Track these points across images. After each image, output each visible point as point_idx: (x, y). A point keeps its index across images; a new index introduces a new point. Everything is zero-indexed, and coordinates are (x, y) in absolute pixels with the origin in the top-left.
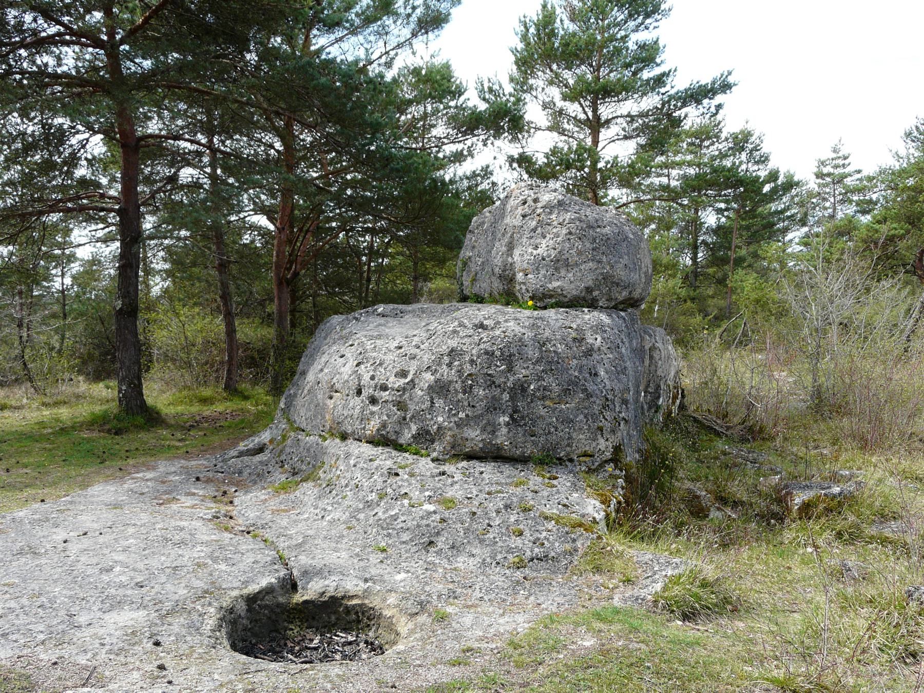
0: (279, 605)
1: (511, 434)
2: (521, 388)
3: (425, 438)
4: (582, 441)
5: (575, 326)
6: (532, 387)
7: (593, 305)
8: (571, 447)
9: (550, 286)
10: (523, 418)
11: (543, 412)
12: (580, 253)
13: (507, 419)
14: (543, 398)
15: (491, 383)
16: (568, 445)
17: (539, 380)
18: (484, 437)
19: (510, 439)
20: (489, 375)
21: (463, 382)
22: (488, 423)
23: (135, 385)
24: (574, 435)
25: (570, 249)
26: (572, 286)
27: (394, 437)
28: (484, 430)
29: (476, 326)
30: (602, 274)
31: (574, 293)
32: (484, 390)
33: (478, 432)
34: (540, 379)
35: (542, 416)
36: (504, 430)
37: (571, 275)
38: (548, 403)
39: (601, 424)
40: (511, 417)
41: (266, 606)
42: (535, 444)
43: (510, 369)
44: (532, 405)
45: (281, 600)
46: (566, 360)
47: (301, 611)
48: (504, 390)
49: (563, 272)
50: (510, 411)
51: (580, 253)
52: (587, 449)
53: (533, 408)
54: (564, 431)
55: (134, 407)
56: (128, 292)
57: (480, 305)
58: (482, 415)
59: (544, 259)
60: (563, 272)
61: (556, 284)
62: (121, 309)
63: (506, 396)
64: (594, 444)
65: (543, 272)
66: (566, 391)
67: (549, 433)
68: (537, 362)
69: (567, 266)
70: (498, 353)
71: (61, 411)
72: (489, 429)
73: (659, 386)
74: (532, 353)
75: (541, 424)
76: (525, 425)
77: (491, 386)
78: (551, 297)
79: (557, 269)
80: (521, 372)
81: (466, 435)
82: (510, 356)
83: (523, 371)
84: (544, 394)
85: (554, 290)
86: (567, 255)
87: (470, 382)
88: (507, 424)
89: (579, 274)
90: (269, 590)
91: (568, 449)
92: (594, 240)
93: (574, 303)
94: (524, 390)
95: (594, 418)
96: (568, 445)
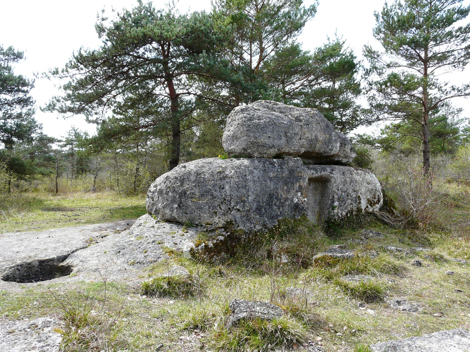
0: (54, 265)
2: (184, 193)
3: (157, 212)
4: (205, 218)
5: (223, 166)
9: (230, 148)
10: (183, 206)
11: (190, 203)
13: (177, 206)
14: (192, 198)
15: (174, 191)
16: (199, 219)
22: (171, 207)
24: (202, 215)
31: (239, 151)
34: (192, 189)
36: (175, 211)
37: (238, 143)
38: (194, 200)
39: (216, 211)
40: (179, 205)
41: (48, 265)
42: (186, 217)
45: (55, 264)
46: (208, 181)
47: (60, 269)
49: (235, 141)
51: (241, 133)
52: (208, 221)
54: (197, 213)
58: (170, 204)
61: (232, 147)
64: (212, 219)
65: (228, 142)
66: (202, 195)
67: (192, 213)
69: (237, 139)
71: (137, 202)
72: (172, 210)
73: (334, 196)
74: (193, 178)
78: (232, 153)
79: (233, 141)
82: (183, 179)
84: (192, 196)
86: (236, 134)
88: (177, 208)
90: (52, 260)
93: (238, 157)
94: (185, 194)
95: (214, 207)
96: (199, 219)
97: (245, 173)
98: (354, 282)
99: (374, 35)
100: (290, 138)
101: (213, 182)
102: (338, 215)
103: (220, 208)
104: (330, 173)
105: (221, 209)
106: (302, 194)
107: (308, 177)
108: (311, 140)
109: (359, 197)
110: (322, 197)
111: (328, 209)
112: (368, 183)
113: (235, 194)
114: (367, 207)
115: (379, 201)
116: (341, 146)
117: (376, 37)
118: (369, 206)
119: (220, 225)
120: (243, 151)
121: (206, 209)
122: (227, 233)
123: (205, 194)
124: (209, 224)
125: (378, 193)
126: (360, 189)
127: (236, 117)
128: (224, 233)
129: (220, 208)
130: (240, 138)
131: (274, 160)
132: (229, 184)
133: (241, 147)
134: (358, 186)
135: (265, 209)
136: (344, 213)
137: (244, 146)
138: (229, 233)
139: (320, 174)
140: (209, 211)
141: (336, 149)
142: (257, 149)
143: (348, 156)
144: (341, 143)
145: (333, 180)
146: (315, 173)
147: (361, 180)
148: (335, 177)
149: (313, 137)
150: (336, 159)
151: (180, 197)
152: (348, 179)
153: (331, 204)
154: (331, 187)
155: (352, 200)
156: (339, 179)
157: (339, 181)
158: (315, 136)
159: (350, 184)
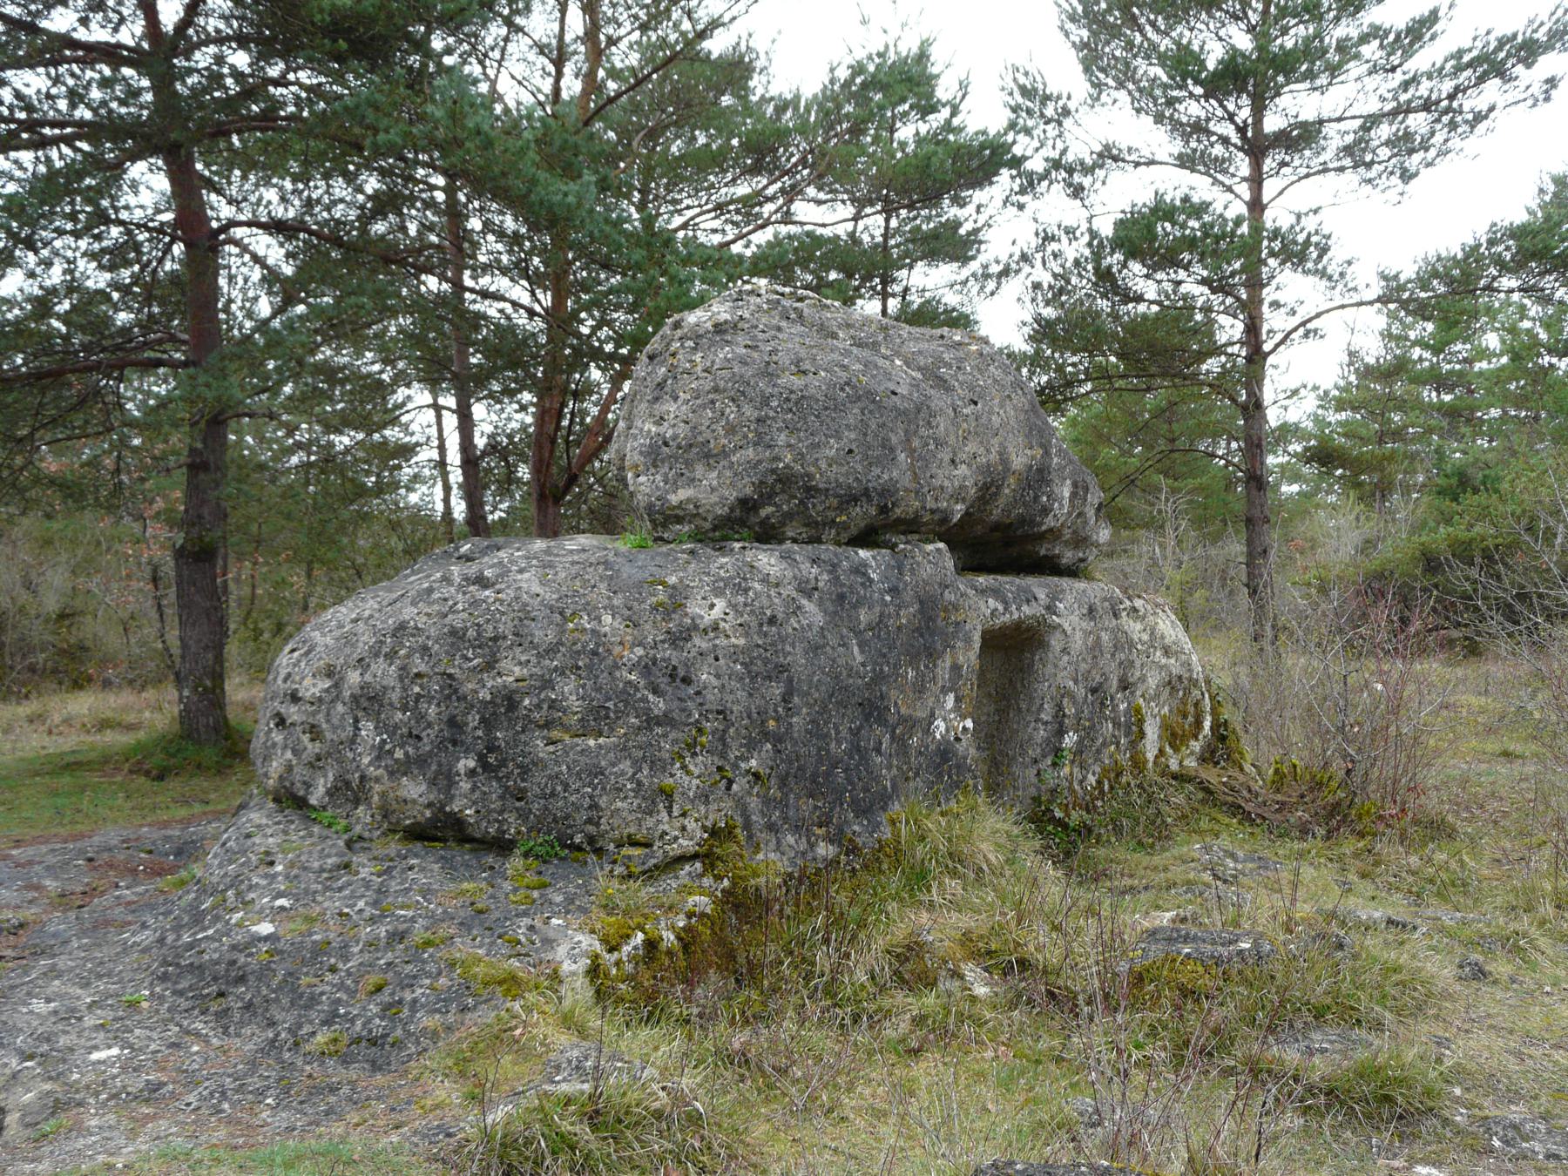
1: (477, 794)
6: (527, 702)
7: (767, 535)
8: (598, 825)
9: (674, 499)
12: (731, 430)
13: (472, 764)
14: (548, 725)
16: (589, 821)
17: (542, 688)
18: (432, 797)
19: (474, 803)
20: (450, 676)
21: (405, 689)
23: (205, 689)
25: (713, 421)
26: (714, 498)
27: (301, 793)
28: (433, 783)
29: (467, 579)
30: (773, 471)
32: (438, 705)
33: (423, 787)
35: (541, 760)
40: (481, 759)
43: (490, 665)
44: (523, 737)
48: (472, 706)
50: (480, 746)
52: (632, 830)
53: (526, 744)
55: (202, 730)
56: (200, 517)
57: (1373, 563)
59: (666, 444)
60: (699, 470)
61: (683, 494)
62: (182, 546)
63: (473, 719)
64: (650, 822)
67: (553, 794)
68: (547, 652)
70: (471, 633)
75: (538, 779)
76: (508, 777)
77: (449, 697)
78: (679, 520)
80: (512, 670)
81: (402, 793)
82: (495, 639)
83: (517, 669)
85: (680, 505)
86: (707, 435)
87: (417, 689)
88: (472, 773)
89: (728, 473)
91: (591, 829)
92: (766, 401)
96: (589, 821)
97: (768, 612)
98: (1321, 1055)
99: (1062, 28)
100: (920, 458)
101: (640, 651)
102: (1071, 788)
103: (684, 767)
104: (1048, 608)
105: (688, 773)
106: (958, 700)
107: (979, 627)
108: (987, 469)
109: (1138, 711)
110: (1002, 712)
111: (1036, 761)
112: (1167, 652)
113: (738, 702)
114: (1161, 752)
115: (1198, 724)
116: (1074, 495)
117: (1067, 35)
118: (1168, 749)
119: (686, 845)
120: (738, 512)
121: (623, 773)
122: (718, 878)
123: (610, 705)
124: (634, 844)
125: (1196, 693)
126: (1143, 679)
127: (698, 357)
128: (707, 881)
129: (684, 767)
130: (724, 453)
131: (862, 553)
132: (711, 659)
133: (732, 495)
134: (1138, 664)
135: (845, 771)
136: (1092, 779)
137: (749, 490)
138: (726, 883)
139: (1016, 616)
140: (639, 783)
141: (1061, 506)
142: (801, 502)
143: (1085, 539)
144: (1075, 485)
145: (1056, 642)
146: (1001, 608)
147: (1145, 637)
148: (1066, 626)
149: (994, 457)
150: (1043, 552)
151: (488, 723)
152: (1105, 637)
153: (1048, 741)
154: (1050, 669)
155: (1117, 724)
156: (1078, 634)
157: (1078, 642)
158: (1000, 454)
159: (1113, 655)
